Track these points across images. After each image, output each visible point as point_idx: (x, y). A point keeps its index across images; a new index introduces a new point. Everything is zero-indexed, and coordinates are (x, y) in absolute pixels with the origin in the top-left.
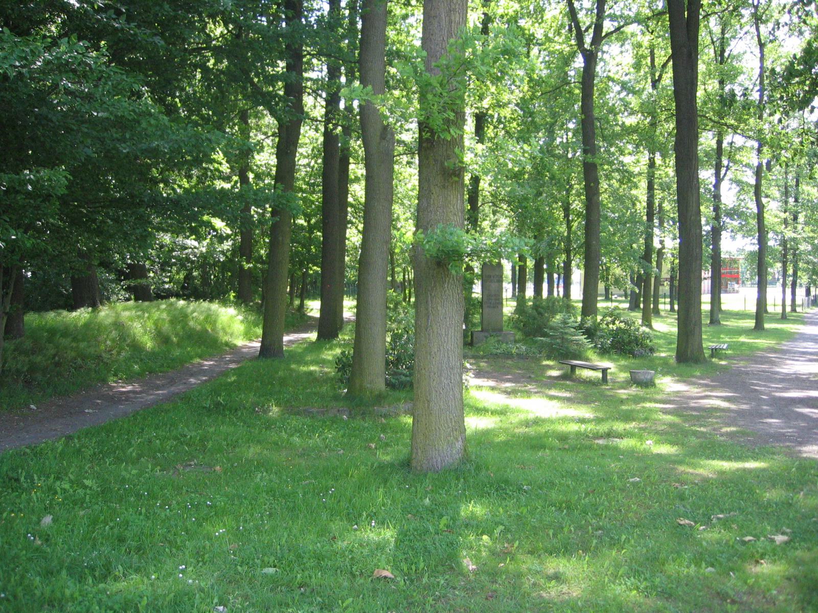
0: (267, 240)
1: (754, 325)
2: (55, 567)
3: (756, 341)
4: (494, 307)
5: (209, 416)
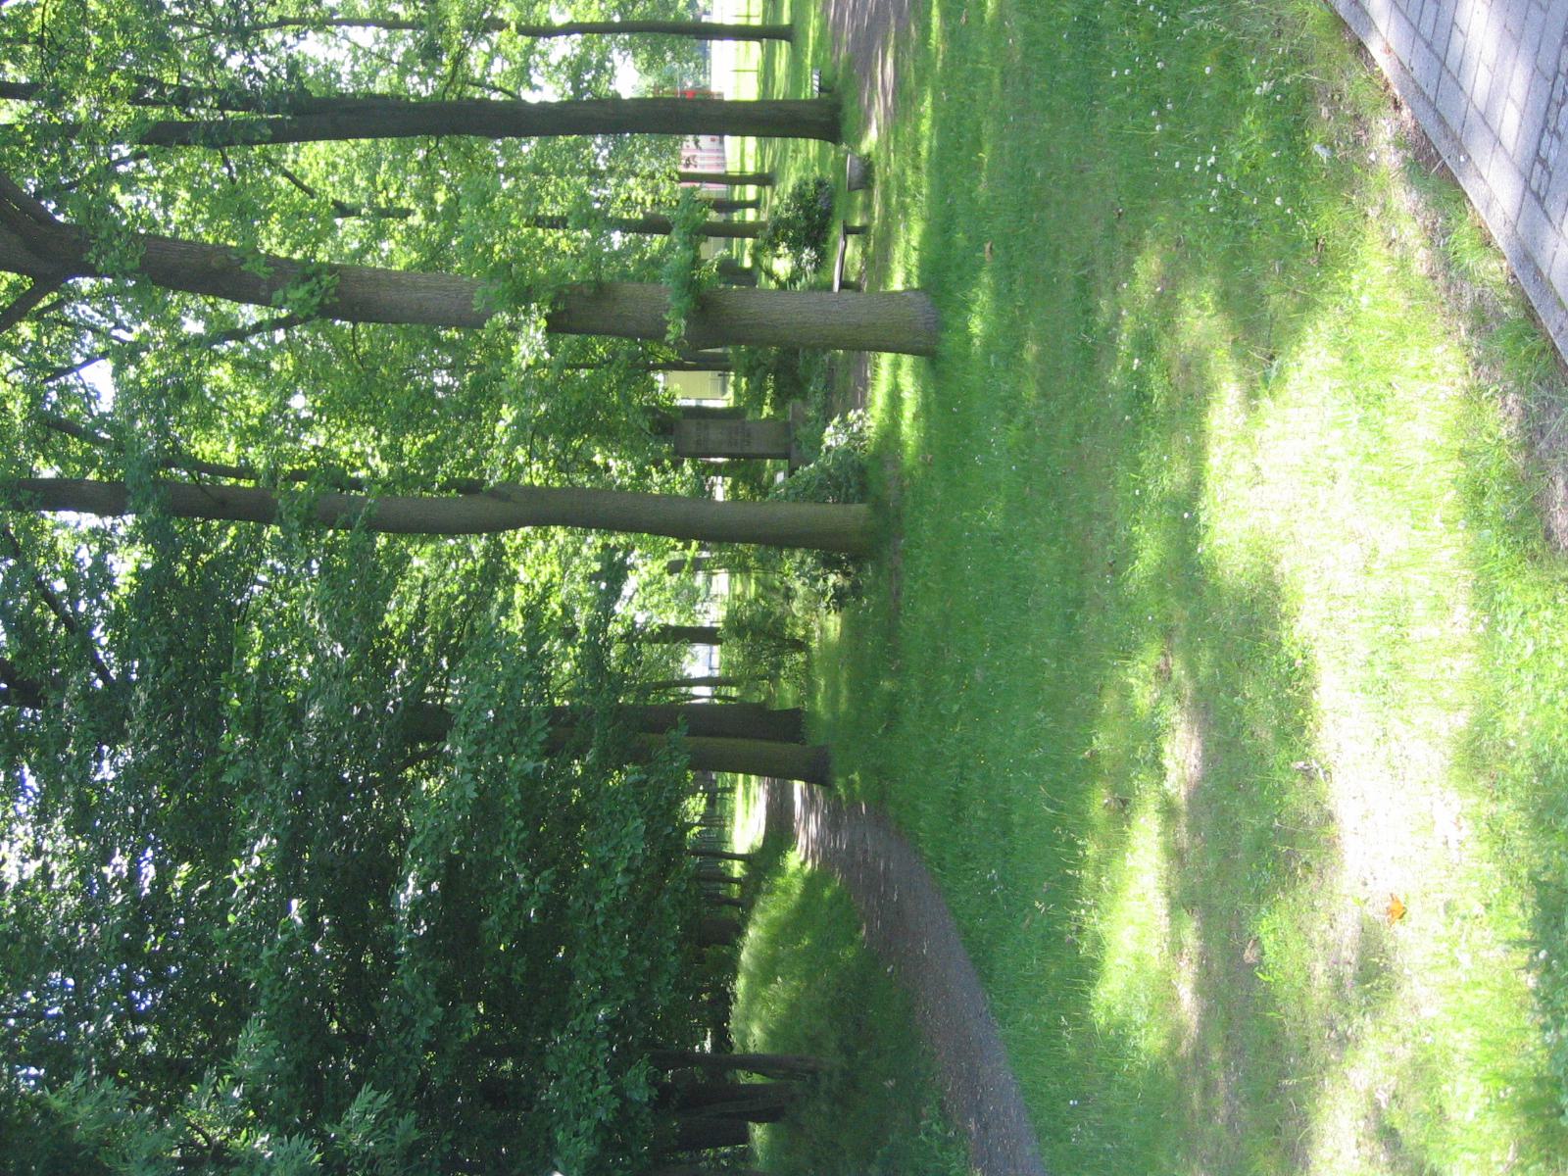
0: (700, 662)
1: (784, 42)
2: (491, 929)
3: (811, 41)
4: (749, 435)
5: (1471, 332)
